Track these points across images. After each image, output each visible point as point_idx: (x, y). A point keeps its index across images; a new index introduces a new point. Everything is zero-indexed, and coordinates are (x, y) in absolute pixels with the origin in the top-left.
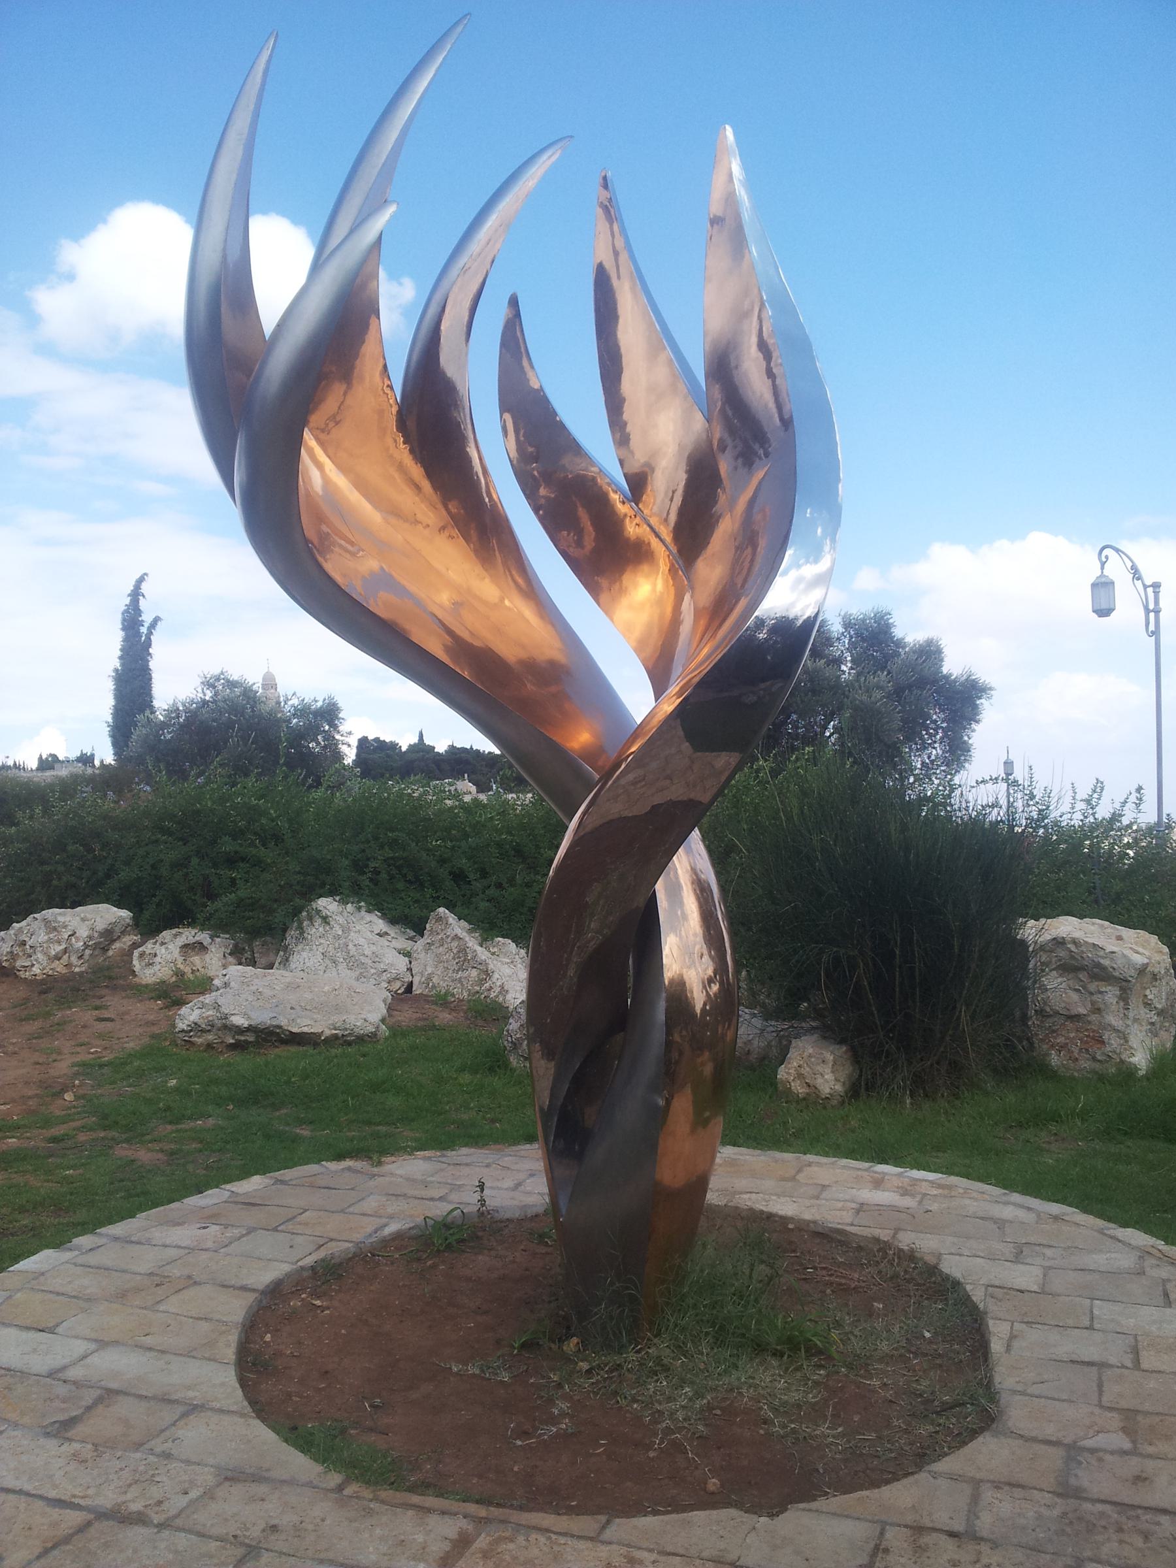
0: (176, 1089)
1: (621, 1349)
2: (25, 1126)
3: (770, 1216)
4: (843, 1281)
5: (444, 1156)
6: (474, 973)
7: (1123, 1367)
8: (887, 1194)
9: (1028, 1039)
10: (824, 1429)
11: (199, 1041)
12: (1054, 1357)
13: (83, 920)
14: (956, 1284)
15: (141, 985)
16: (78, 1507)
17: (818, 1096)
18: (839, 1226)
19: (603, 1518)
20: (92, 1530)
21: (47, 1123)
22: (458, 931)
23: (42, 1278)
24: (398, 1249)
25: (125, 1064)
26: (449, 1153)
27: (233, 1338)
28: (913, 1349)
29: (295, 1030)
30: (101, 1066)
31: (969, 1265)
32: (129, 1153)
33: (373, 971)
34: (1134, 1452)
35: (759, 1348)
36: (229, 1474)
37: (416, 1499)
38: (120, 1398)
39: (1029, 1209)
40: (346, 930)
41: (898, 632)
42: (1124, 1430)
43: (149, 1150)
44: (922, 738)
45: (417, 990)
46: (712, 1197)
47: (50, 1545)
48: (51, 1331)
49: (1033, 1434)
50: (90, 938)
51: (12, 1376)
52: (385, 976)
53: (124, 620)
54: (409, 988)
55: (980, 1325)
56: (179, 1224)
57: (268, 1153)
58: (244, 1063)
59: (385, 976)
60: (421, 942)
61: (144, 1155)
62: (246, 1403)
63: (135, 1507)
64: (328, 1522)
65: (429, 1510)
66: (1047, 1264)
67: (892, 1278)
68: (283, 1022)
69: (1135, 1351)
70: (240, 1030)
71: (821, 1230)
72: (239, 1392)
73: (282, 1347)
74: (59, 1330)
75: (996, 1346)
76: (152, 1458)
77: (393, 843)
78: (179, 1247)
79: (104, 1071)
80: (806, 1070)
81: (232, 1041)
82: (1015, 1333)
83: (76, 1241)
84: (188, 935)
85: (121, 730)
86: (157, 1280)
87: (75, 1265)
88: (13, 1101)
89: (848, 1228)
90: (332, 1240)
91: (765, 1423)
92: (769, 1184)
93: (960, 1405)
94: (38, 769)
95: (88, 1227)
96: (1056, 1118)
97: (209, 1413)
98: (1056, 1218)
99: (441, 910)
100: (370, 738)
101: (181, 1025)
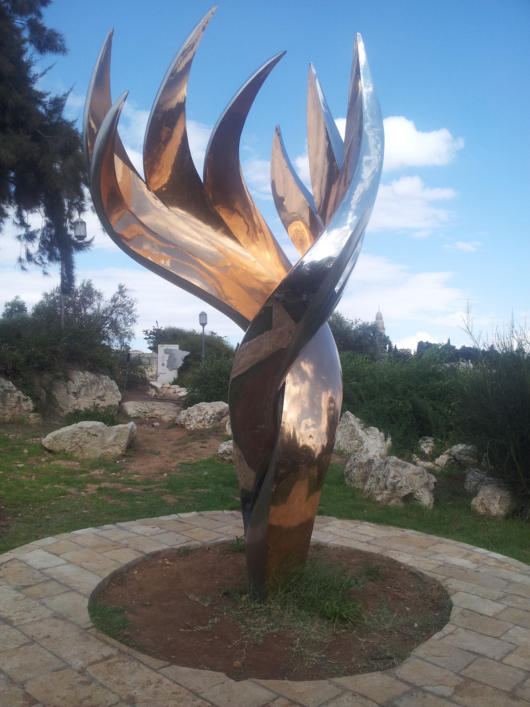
3: (395, 562)
6: (357, 442)
11: (227, 458)
12: (461, 647)
13: (212, 407)
18: (422, 571)
22: (353, 422)
25: (196, 465)
41: (93, 287)
48: (58, 555)
50: (213, 415)
74: (61, 556)
80: (485, 502)
89: (425, 573)
90: (195, 540)
91: (291, 645)
99: (348, 412)
100: (424, 341)
101: (220, 451)
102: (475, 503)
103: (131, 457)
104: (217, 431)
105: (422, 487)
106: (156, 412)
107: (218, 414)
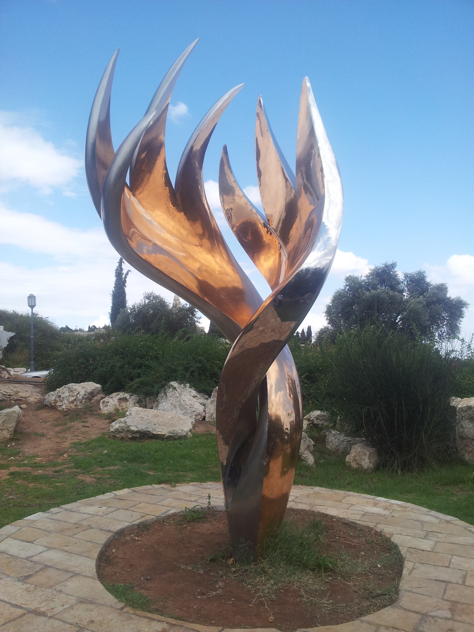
0: (106, 454)
1: (248, 564)
2: (46, 466)
3: (326, 515)
4: (350, 543)
5: (201, 485)
7: (458, 584)
8: (378, 509)
9: (456, 448)
10: (324, 601)
13: (83, 388)
14: (396, 546)
15: (102, 414)
16: (21, 607)
17: (362, 469)
19: (221, 628)
20: (25, 617)
21: (55, 465)
23: (34, 523)
24: (173, 520)
25: (90, 444)
26: (203, 484)
27: (99, 550)
28: (371, 571)
29: (155, 433)
30: (81, 444)
31: (402, 539)
32: (83, 478)
33: (190, 411)
34: (452, 619)
35: (304, 567)
36: (82, 600)
37: (150, 615)
38: (50, 569)
39: (438, 518)
40: (180, 394)
41: (428, 280)
42: (450, 609)
43: (90, 477)
44: (437, 323)
45: (207, 419)
46: (290, 505)
47: (7, 621)
48: (32, 542)
49: (410, 608)
50: (85, 395)
51: (12, 558)
52: (194, 413)
53: (116, 273)
54: (204, 418)
55: (403, 563)
56: (91, 505)
57: (133, 480)
58: (134, 445)
59: (194, 413)
60: (210, 400)
61: (88, 479)
62: (96, 574)
63: (42, 610)
64: (113, 621)
65: (154, 620)
66: (437, 540)
67: (370, 543)
68: (150, 429)
69: (465, 577)
70: (134, 432)
71: (346, 522)
72: (95, 570)
73: (118, 554)
74: (35, 542)
75: (405, 572)
76: (55, 592)
77: (200, 362)
78: (89, 514)
79: (81, 446)
80: (357, 458)
81: (131, 436)
82: (415, 567)
83: (51, 510)
84: (122, 395)
85: (114, 316)
86: (77, 526)
87: (48, 518)
88: (44, 456)
89: (357, 522)
90: (148, 515)
91: (300, 597)
92: (329, 503)
93: (383, 595)
94: (88, 331)
95: (58, 505)
96: (462, 482)
97: (81, 577)
98: (448, 522)
101: (112, 430)
102: (349, 460)
103: (18, 439)
104: (91, 411)
105: (306, 449)
106: (21, 394)
107: (89, 394)
